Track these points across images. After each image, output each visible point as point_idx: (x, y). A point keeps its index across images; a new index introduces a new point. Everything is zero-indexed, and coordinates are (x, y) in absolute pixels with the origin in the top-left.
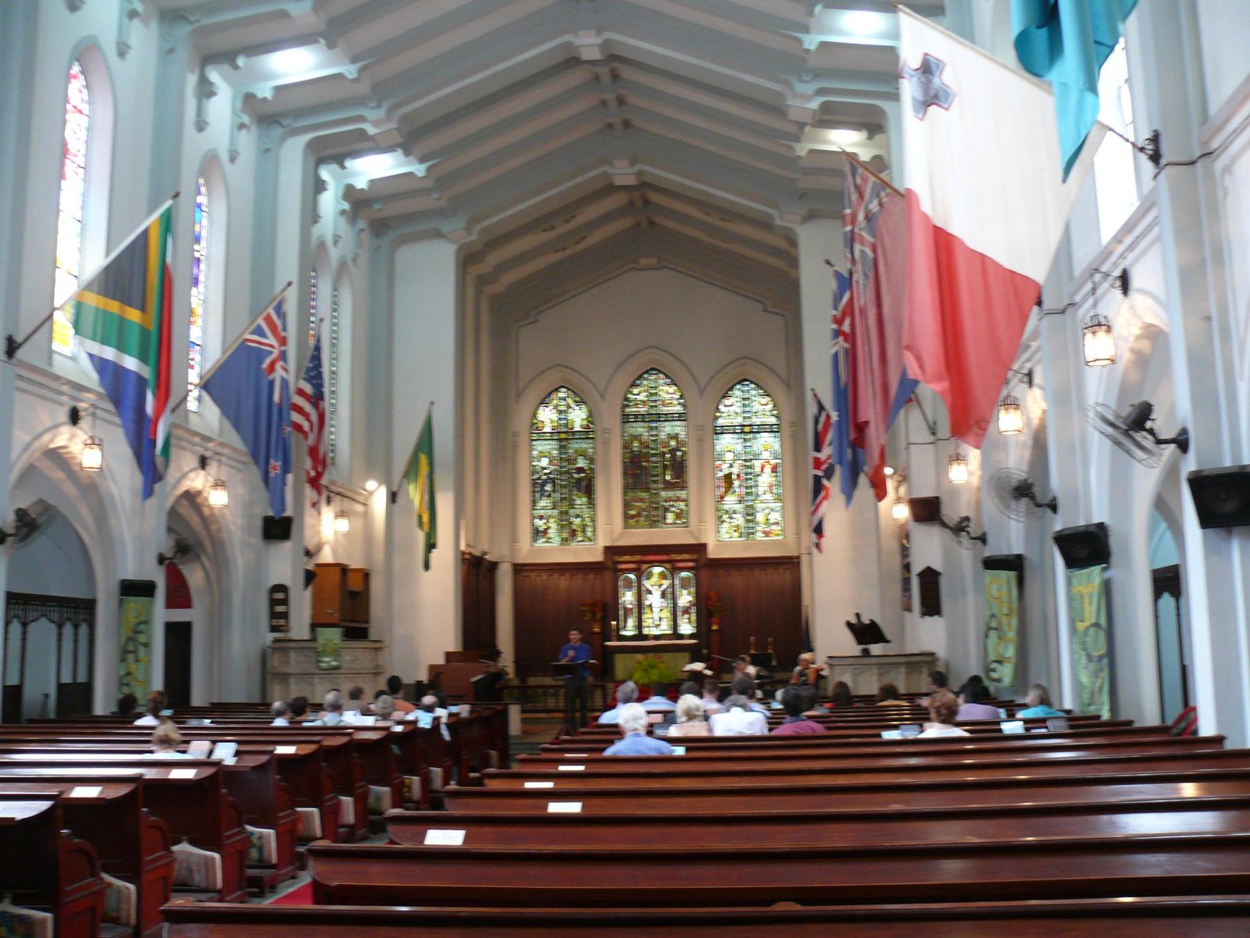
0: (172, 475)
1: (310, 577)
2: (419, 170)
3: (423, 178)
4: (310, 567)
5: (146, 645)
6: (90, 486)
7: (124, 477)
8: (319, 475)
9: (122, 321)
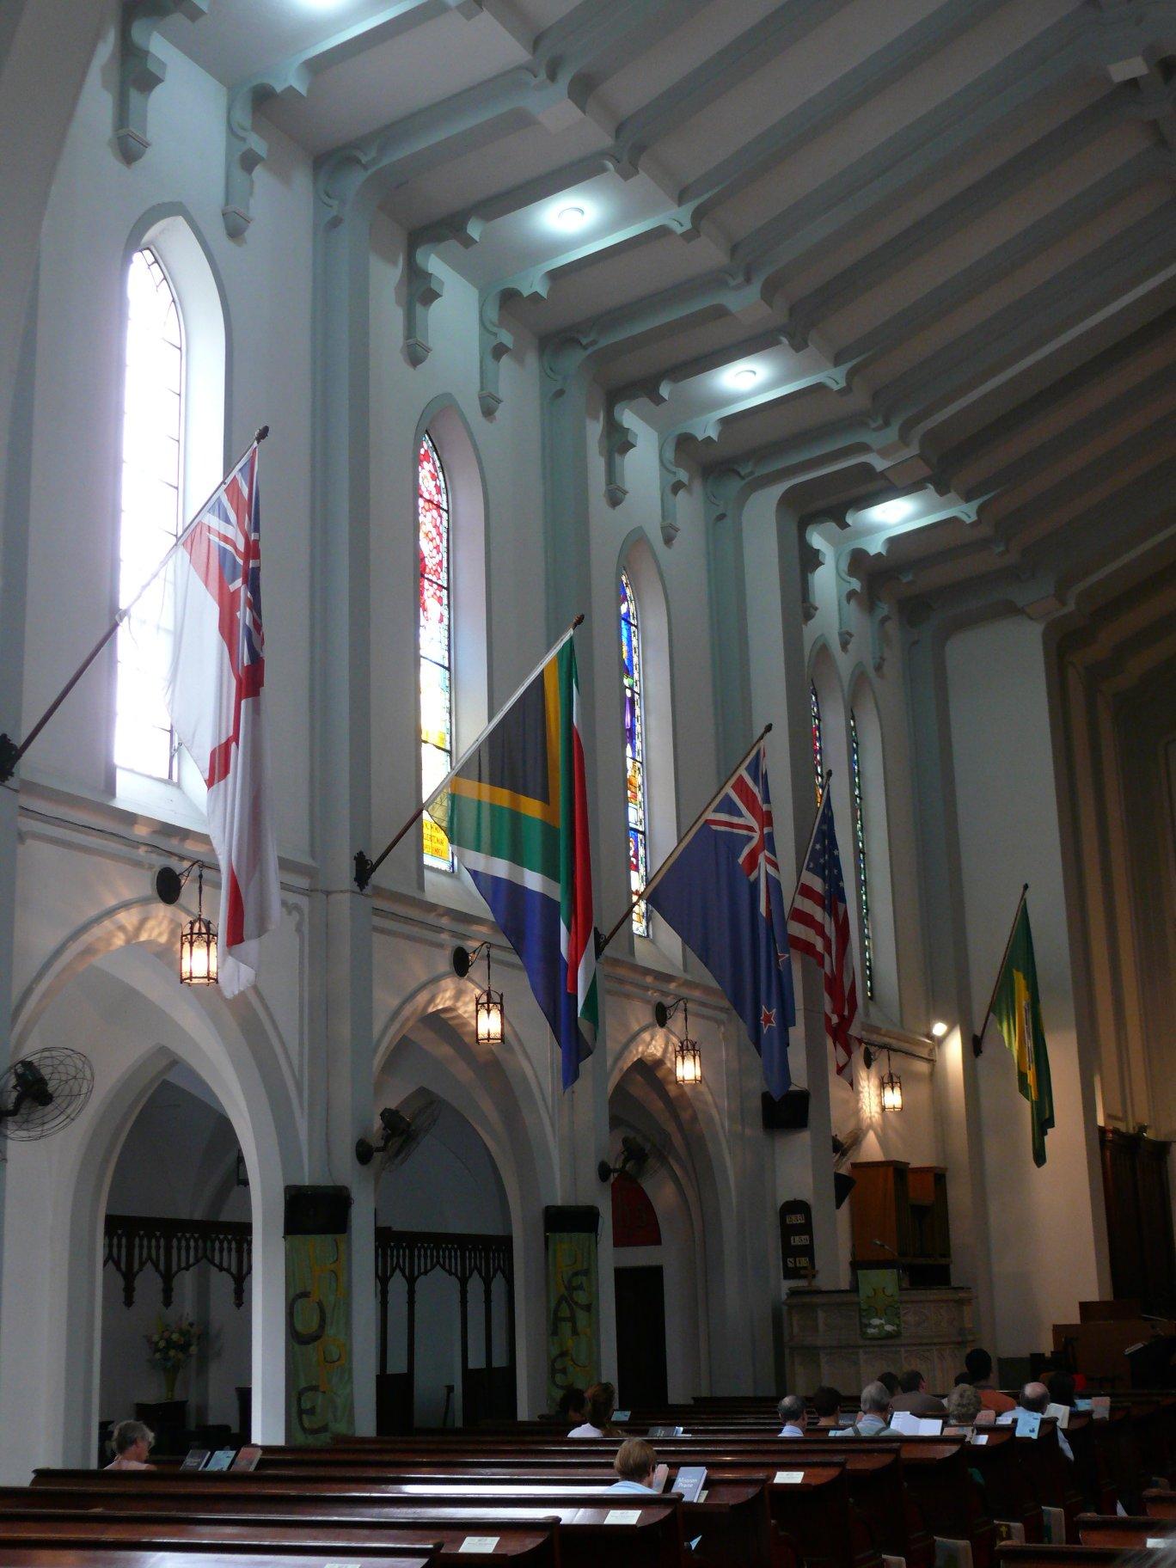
0: (612, 1035)
1: (843, 1186)
2: (966, 511)
3: (973, 524)
4: (843, 1171)
5: (588, 1308)
6: (491, 1063)
7: (541, 1052)
8: (846, 1022)
9: (516, 817)
